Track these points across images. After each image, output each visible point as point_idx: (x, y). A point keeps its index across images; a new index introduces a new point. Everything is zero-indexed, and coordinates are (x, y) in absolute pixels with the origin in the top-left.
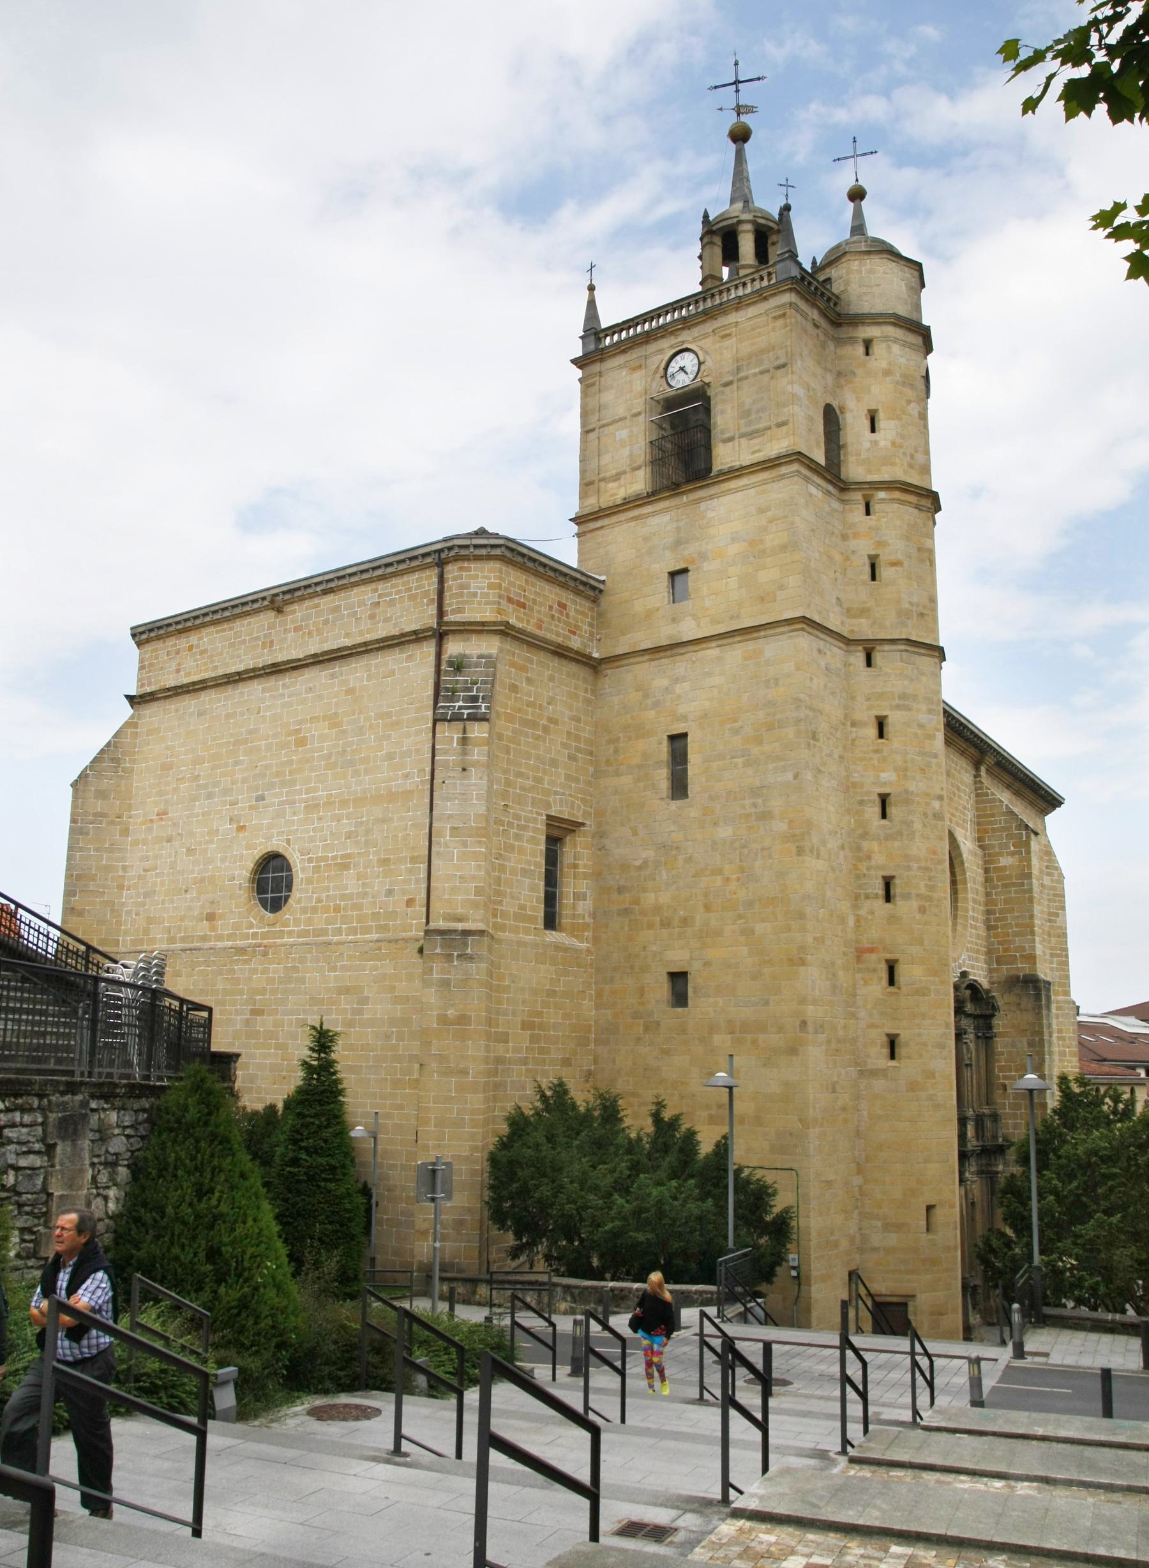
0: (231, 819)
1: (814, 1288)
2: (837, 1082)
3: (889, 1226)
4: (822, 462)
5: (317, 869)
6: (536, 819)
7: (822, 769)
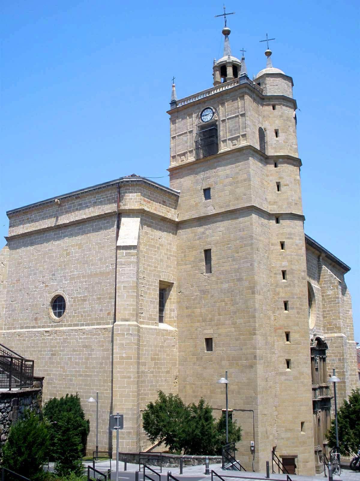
0: (43, 282)
1: (260, 454)
2: (267, 378)
3: (288, 430)
4: (259, 149)
5: (75, 301)
6: (155, 282)
7: (261, 261)
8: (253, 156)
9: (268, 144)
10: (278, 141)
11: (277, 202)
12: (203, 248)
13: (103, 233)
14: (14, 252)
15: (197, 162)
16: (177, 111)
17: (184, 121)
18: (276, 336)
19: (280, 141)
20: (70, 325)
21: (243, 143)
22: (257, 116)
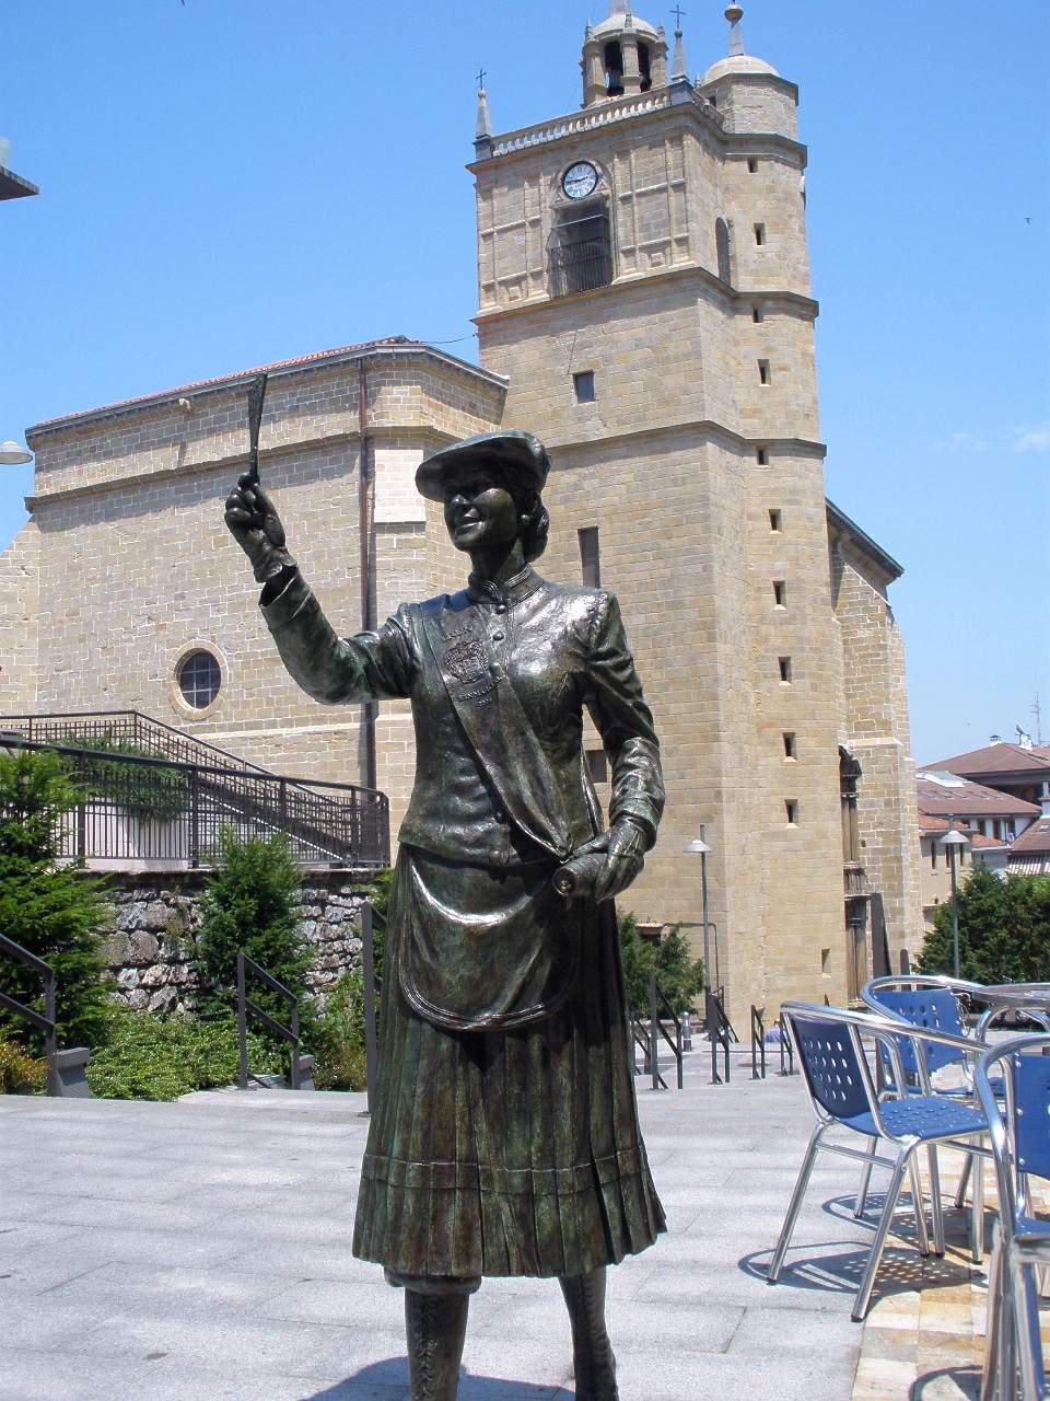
0: (149, 618)
4: (716, 274)
5: (246, 665)
8: (705, 295)
9: (738, 261)
10: (762, 254)
11: (760, 411)
12: (577, 524)
13: (319, 487)
14: (56, 537)
15: (556, 303)
16: (494, 166)
17: (517, 192)
18: (760, 744)
19: (769, 255)
20: (233, 728)
21: (680, 262)
22: (711, 188)
